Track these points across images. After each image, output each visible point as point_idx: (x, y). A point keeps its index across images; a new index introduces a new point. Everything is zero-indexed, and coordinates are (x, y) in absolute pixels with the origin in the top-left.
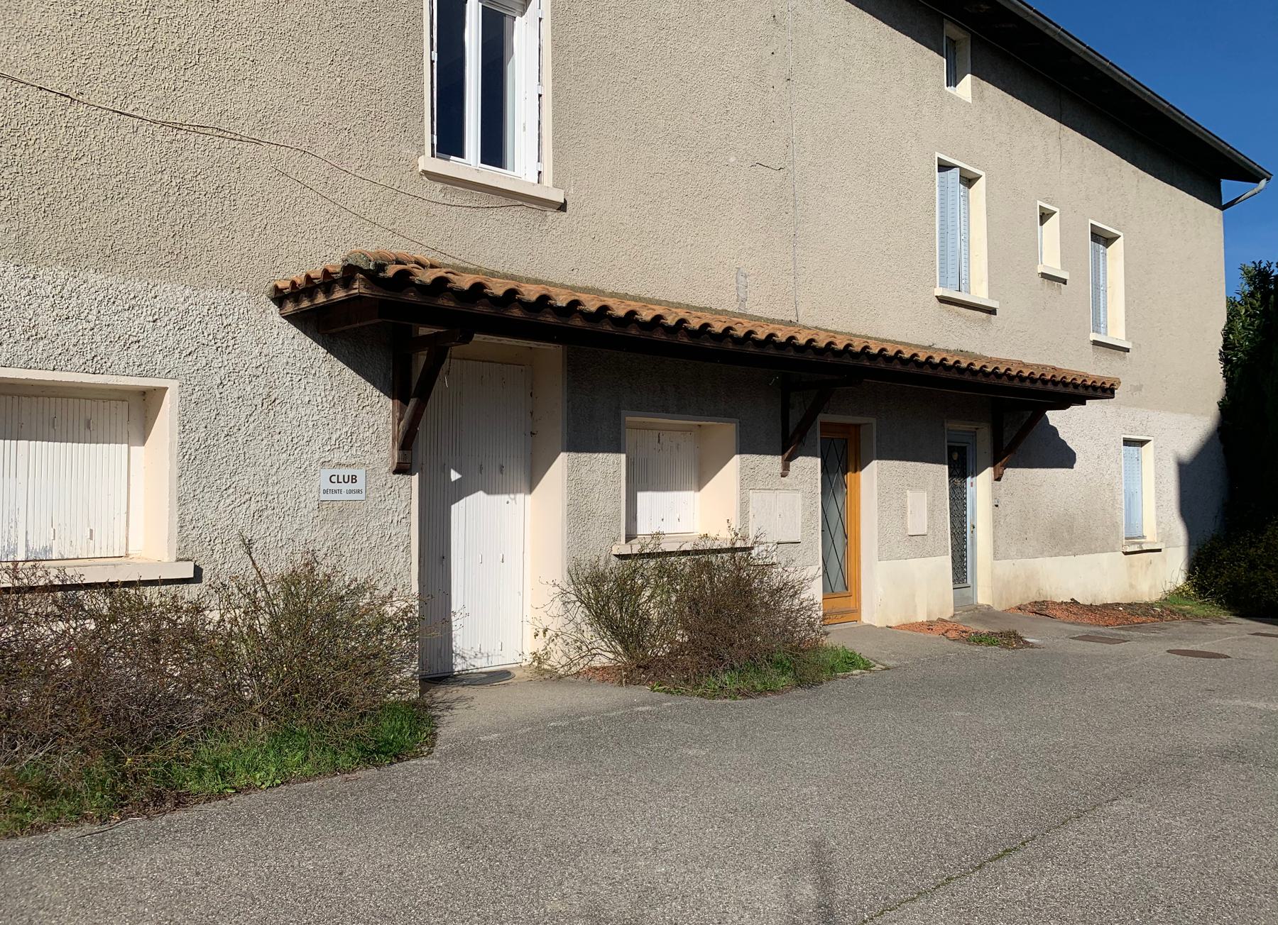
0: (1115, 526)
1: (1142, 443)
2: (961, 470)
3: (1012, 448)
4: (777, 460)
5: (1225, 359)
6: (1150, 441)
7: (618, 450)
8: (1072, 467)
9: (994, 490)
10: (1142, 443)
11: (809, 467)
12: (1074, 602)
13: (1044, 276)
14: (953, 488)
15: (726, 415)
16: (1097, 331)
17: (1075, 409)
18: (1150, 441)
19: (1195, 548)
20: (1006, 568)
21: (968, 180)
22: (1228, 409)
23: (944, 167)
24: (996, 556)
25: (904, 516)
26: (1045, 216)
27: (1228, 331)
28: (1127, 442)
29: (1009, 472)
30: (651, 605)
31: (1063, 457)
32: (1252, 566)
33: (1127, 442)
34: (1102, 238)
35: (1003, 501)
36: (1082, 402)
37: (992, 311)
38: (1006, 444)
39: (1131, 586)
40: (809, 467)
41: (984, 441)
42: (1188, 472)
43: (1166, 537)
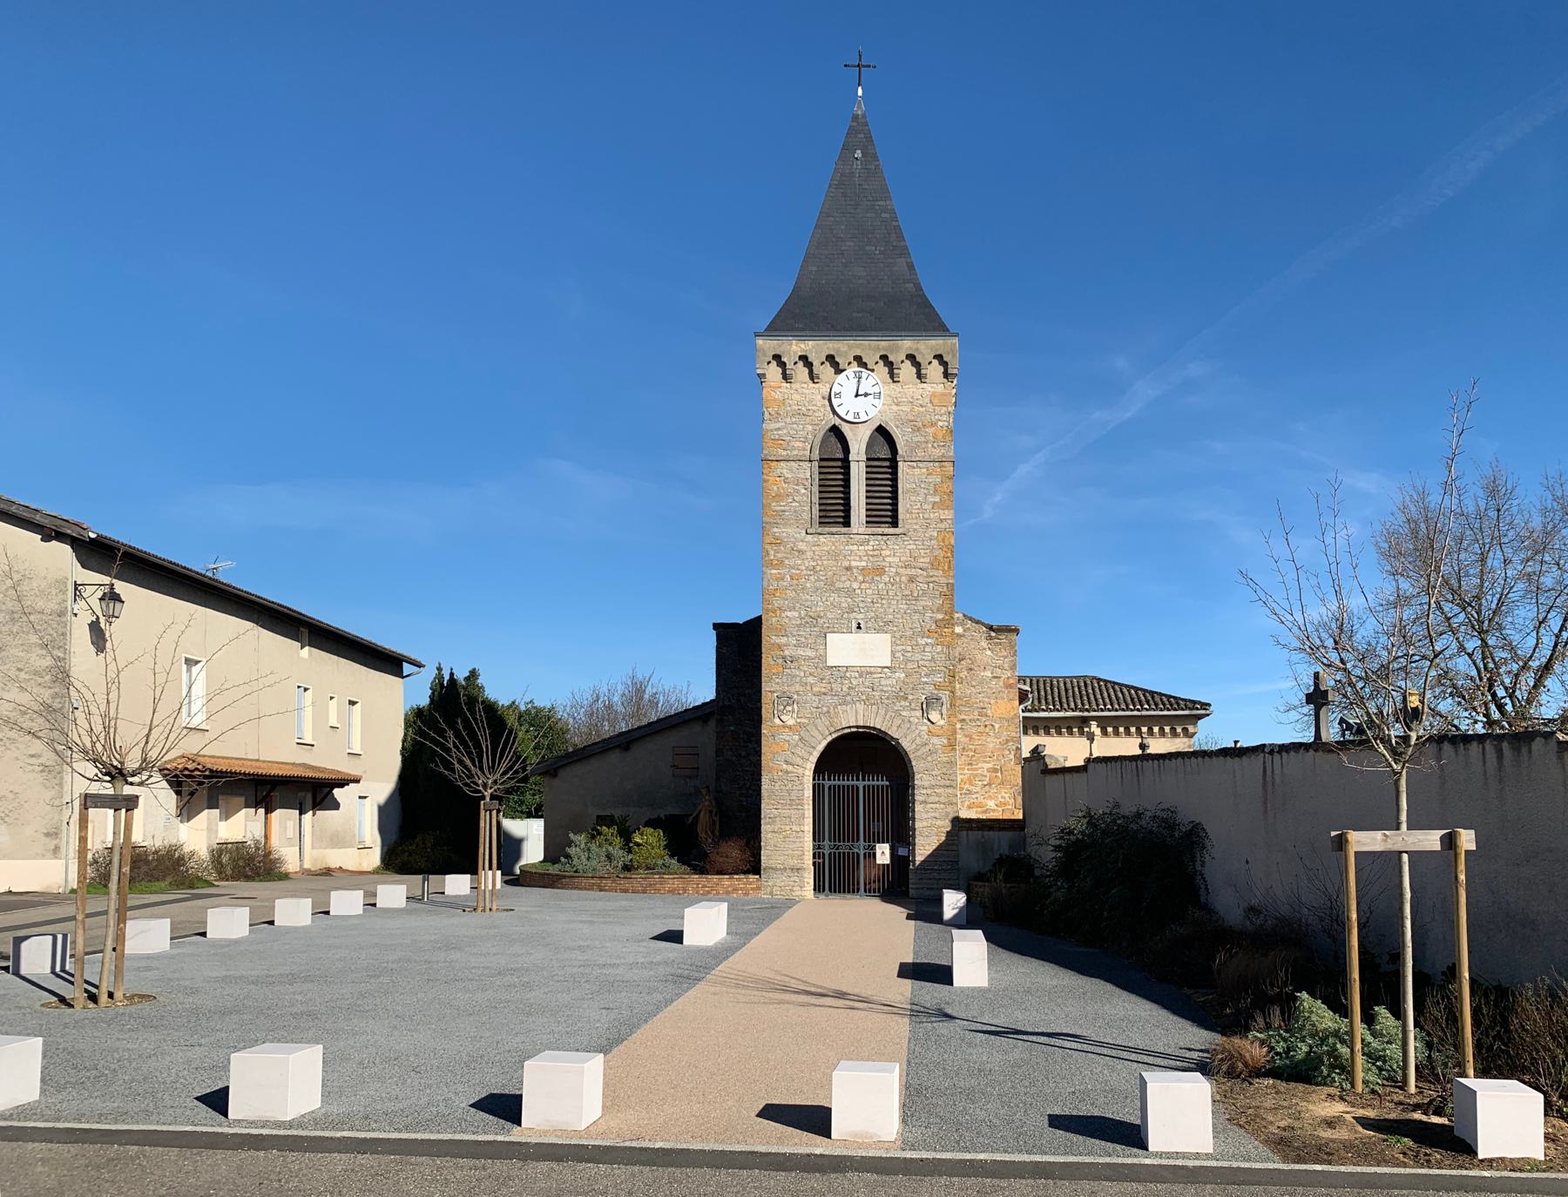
0: (354, 835)
1: (365, 797)
2: (268, 811)
3: (319, 804)
4: (254, 809)
5: (402, 754)
6: (200, 661)
7: (217, 808)
8: (338, 809)
9: (313, 820)
10: (365, 797)
11: (262, 811)
12: (341, 868)
13: (331, 727)
14: (266, 818)
15: (241, 795)
16: (349, 748)
17: (346, 787)
18: (200, 661)
19: (386, 848)
20: (318, 853)
21: (306, 690)
22: (403, 778)
23: (299, 687)
24: (313, 848)
25: (286, 831)
26: (332, 698)
27: (404, 741)
28: (360, 797)
29: (318, 812)
30: (225, 859)
31: (335, 805)
32: (410, 855)
33: (360, 797)
34: (352, 703)
35: (316, 824)
36: (348, 785)
37: (313, 745)
38: (318, 800)
39: (360, 864)
40: (262, 811)
41: (309, 801)
42: (382, 810)
43: (374, 842)
